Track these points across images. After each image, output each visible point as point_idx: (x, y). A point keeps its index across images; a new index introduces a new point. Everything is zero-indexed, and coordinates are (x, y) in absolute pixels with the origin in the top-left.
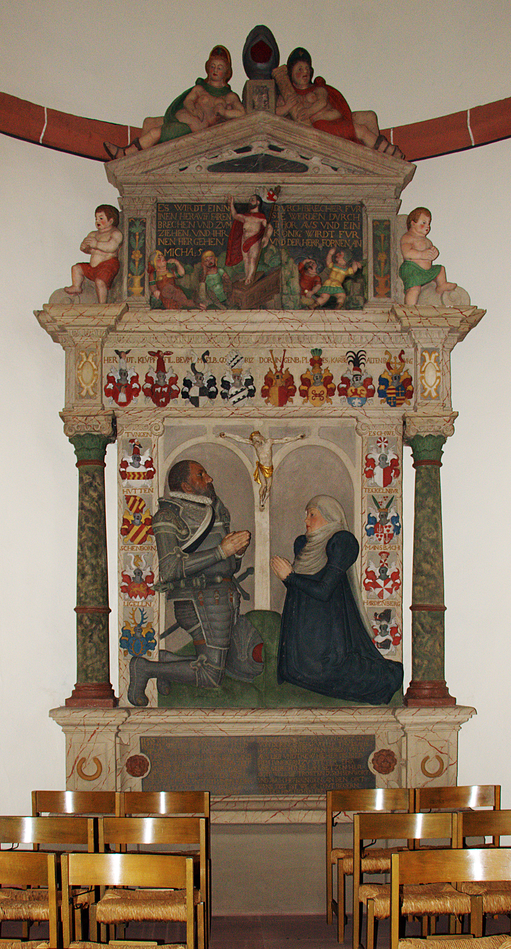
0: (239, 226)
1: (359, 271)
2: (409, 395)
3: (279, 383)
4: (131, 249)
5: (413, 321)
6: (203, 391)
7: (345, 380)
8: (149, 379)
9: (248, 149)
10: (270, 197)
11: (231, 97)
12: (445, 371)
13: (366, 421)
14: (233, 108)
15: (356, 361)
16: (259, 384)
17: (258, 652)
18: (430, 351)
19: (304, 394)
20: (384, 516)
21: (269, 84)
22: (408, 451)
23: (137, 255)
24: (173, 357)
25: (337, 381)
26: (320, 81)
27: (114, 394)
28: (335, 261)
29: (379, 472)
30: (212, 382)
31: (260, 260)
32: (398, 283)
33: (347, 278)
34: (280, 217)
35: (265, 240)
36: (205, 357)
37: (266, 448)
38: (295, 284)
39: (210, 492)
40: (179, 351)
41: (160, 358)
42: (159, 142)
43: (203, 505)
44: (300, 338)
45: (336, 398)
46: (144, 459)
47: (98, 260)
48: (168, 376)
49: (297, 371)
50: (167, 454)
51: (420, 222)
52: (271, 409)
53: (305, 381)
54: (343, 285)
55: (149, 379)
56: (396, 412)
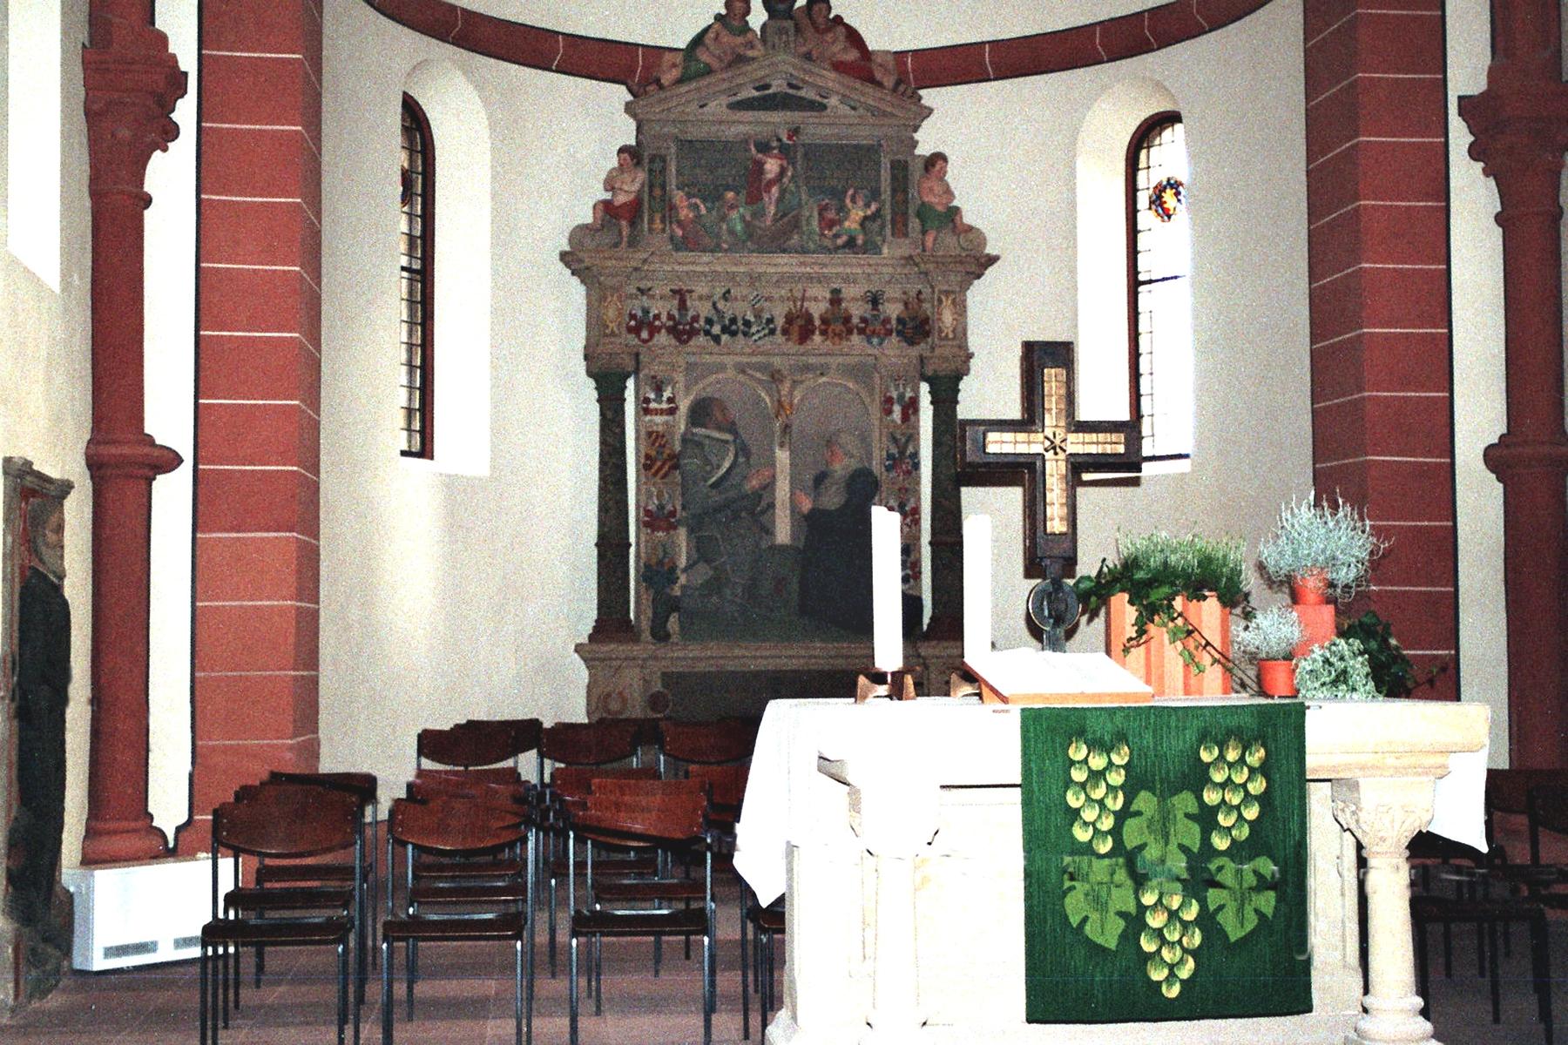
0: (760, 166)
1: (878, 210)
2: (927, 334)
3: (800, 322)
4: (651, 187)
5: (931, 267)
6: (725, 330)
7: (863, 320)
8: (671, 317)
9: (767, 87)
10: (790, 138)
11: (749, 35)
12: (961, 309)
13: (884, 359)
14: (752, 47)
15: (875, 300)
16: (780, 322)
17: (780, 583)
18: (947, 293)
19: (824, 333)
20: (902, 453)
21: (789, 24)
22: (924, 388)
23: (657, 192)
24: (695, 295)
25: (855, 320)
26: (838, 19)
27: (636, 331)
28: (853, 201)
29: (897, 409)
30: (733, 321)
31: (780, 200)
32: (914, 224)
33: (866, 218)
34: (799, 155)
35: (785, 180)
36: (726, 296)
37: (787, 384)
38: (815, 223)
39: (732, 428)
40: (701, 289)
41: (681, 295)
42: (680, 81)
43: (727, 442)
44: (821, 279)
45: (856, 339)
46: (667, 394)
47: (621, 199)
48: (691, 313)
49: (817, 309)
50: (687, 388)
51: (938, 167)
52: (792, 347)
53: (824, 321)
54: (862, 225)
55: (671, 317)
56: (914, 352)
